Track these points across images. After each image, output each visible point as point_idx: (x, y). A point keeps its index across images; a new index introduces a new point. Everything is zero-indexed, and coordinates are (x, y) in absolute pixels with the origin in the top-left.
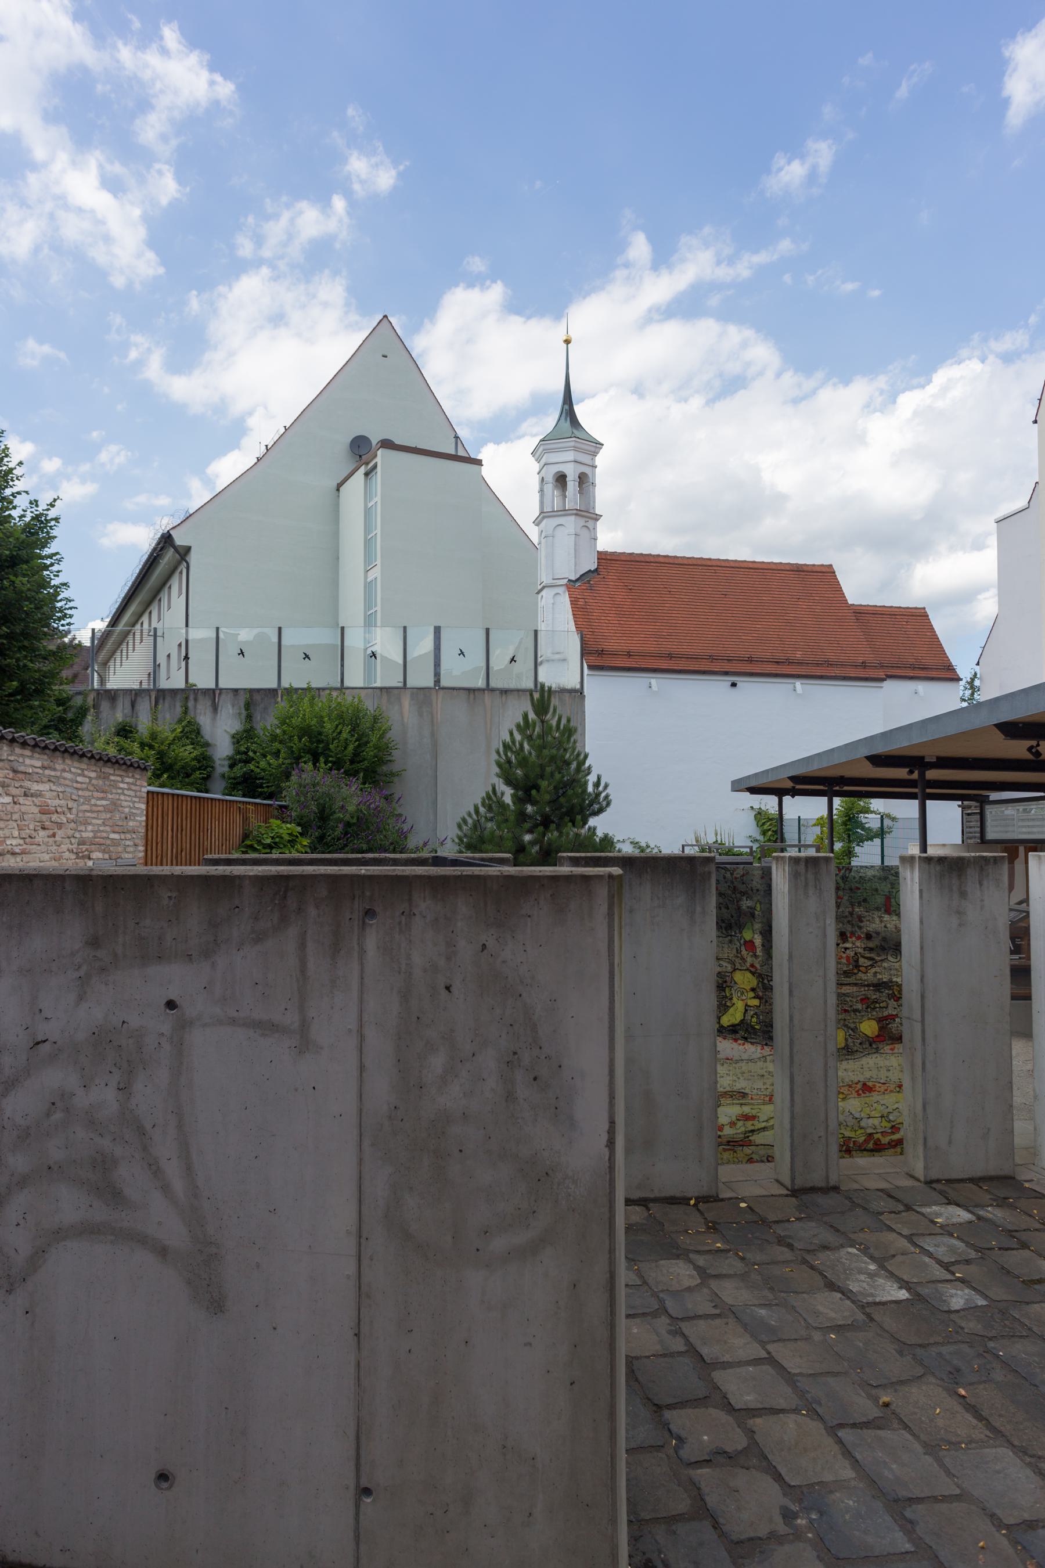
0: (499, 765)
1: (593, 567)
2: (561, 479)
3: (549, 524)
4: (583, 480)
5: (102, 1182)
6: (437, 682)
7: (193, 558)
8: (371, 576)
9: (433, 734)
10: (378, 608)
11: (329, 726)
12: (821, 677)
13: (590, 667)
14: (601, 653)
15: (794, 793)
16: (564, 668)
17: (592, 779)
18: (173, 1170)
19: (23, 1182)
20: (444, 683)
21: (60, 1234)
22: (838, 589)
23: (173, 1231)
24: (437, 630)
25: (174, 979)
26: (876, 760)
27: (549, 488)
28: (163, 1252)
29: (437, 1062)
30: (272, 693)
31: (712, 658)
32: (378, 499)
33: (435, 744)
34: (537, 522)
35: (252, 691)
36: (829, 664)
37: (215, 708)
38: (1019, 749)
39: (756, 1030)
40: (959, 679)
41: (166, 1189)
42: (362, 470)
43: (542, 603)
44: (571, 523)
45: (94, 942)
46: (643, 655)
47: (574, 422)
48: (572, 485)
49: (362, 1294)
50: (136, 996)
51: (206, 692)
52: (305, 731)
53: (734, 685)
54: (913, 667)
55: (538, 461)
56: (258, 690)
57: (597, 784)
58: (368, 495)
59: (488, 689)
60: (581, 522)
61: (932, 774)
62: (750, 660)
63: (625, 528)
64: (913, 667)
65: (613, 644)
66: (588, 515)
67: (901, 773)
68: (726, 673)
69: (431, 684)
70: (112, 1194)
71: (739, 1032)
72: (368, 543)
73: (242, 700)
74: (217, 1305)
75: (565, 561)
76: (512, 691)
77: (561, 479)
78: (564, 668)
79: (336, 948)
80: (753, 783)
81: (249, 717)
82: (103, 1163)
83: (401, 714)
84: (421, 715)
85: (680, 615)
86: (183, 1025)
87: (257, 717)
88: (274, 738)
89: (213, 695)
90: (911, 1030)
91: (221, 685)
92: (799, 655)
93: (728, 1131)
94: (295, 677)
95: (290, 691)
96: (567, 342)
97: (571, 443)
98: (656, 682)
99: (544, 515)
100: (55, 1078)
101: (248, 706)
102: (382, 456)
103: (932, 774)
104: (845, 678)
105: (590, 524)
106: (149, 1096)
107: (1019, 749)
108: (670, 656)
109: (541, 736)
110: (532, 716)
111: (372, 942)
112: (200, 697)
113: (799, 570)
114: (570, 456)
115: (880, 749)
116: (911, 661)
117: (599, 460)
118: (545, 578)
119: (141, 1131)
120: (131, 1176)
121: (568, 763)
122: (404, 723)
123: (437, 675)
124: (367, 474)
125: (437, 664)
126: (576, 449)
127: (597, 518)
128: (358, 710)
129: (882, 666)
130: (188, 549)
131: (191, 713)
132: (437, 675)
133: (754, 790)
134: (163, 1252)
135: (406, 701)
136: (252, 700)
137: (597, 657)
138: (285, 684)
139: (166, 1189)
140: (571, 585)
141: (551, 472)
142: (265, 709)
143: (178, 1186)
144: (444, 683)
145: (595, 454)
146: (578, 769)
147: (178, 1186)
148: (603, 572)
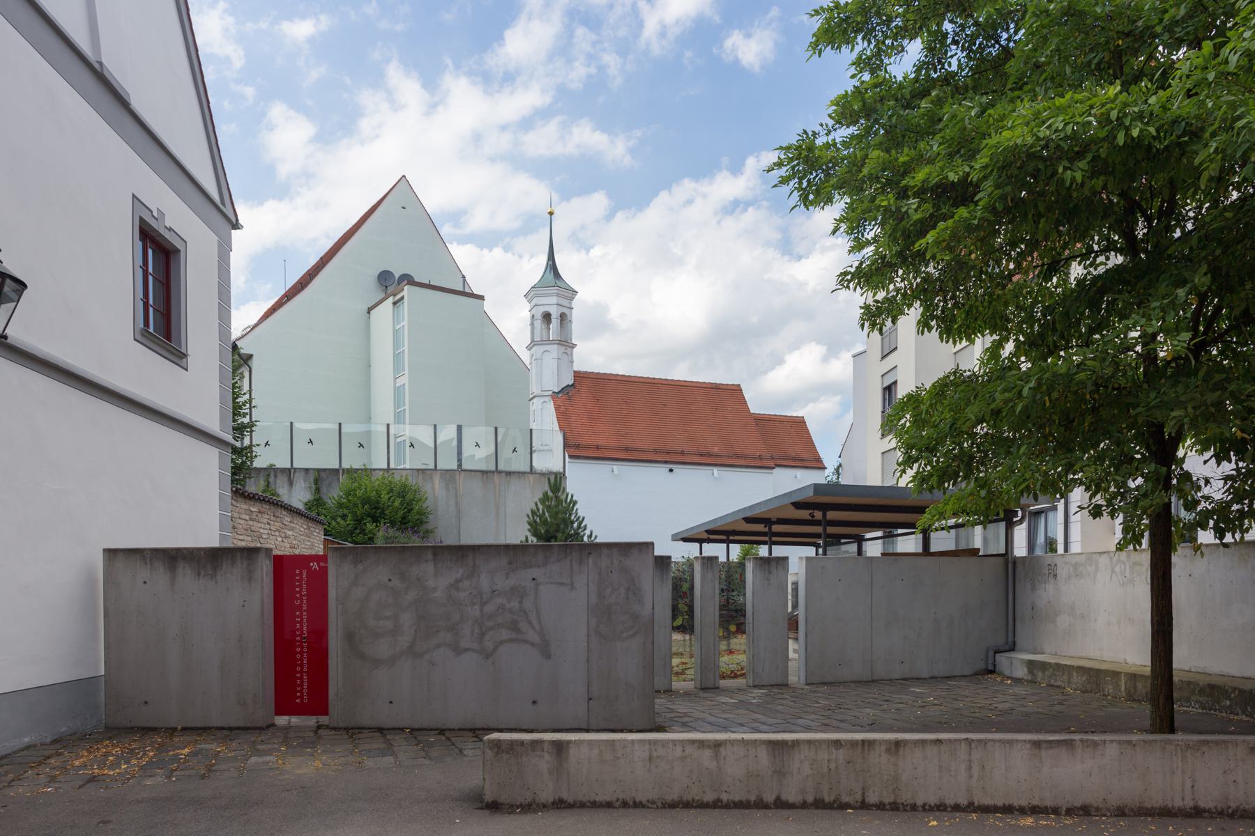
0: (529, 524)
1: (571, 383)
2: (547, 317)
3: (538, 350)
4: (563, 317)
5: (514, 626)
6: (460, 465)
7: (255, 363)
8: (399, 382)
9: (457, 504)
10: (407, 407)
11: (385, 497)
12: (731, 466)
13: (570, 457)
14: (578, 446)
15: (709, 541)
16: (551, 457)
17: (587, 532)
18: (535, 623)
19: (491, 629)
20: (464, 467)
21: (502, 642)
22: (743, 402)
23: (535, 638)
24: (459, 428)
25: (534, 572)
26: (748, 520)
27: (538, 323)
28: (533, 644)
29: (608, 591)
30: (335, 472)
31: (656, 451)
32: (405, 323)
33: (459, 511)
34: (529, 348)
35: (319, 470)
36: (737, 457)
37: (291, 483)
38: (804, 514)
39: (687, 628)
40: (825, 468)
41: (533, 628)
42: (391, 300)
43: (532, 409)
44: (554, 349)
45: (510, 563)
46: (607, 448)
47: (557, 274)
48: (555, 323)
49: (589, 650)
50: (524, 577)
51: (283, 470)
52: (366, 501)
53: (671, 470)
54: (794, 459)
55: (530, 301)
56: (324, 470)
57: (590, 536)
58: (396, 319)
59: (497, 471)
60: (562, 349)
61: (776, 528)
62: (682, 453)
63: (594, 355)
64: (794, 459)
65: (584, 441)
66: (566, 344)
67: (760, 527)
68: (666, 462)
69: (455, 466)
70: (518, 631)
71: (681, 629)
72: (397, 357)
73: (312, 477)
74: (549, 657)
75: (548, 376)
76: (514, 473)
77: (547, 317)
78: (551, 457)
79: (581, 562)
80: (685, 535)
81: (318, 490)
82: (515, 622)
83: (433, 488)
84: (448, 489)
85: (628, 416)
86: (538, 585)
87: (324, 489)
88: (341, 505)
89: (289, 473)
90: (749, 628)
91: (295, 466)
92: (716, 449)
93: (675, 669)
94: (352, 460)
95: (350, 471)
96: (551, 214)
97: (554, 290)
98: (617, 468)
99: (533, 344)
100: (499, 600)
101: (316, 481)
102: (407, 291)
103: (776, 528)
104: (747, 467)
105: (568, 351)
106: (528, 604)
107: (804, 514)
108: (627, 449)
109: (556, 506)
110: (550, 494)
111: (591, 561)
112: (279, 474)
113: (717, 388)
114: (554, 300)
115: (748, 514)
116: (793, 455)
117: (575, 303)
118: (535, 389)
119: (526, 613)
120: (523, 626)
121: (573, 523)
122: (435, 494)
123: (460, 460)
124: (395, 303)
125: (460, 453)
126: (558, 295)
127: (573, 346)
128: (405, 486)
129: (773, 458)
130: (251, 356)
131: (272, 486)
132: (460, 460)
133: (685, 540)
134: (533, 644)
135: (437, 478)
136: (320, 478)
137: (575, 449)
138: (346, 465)
139: (533, 628)
140: (555, 396)
141: (539, 312)
142: (330, 484)
143: (537, 627)
144: (464, 467)
145: (572, 299)
146: (579, 527)
147: (537, 627)
148: (578, 386)
